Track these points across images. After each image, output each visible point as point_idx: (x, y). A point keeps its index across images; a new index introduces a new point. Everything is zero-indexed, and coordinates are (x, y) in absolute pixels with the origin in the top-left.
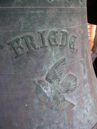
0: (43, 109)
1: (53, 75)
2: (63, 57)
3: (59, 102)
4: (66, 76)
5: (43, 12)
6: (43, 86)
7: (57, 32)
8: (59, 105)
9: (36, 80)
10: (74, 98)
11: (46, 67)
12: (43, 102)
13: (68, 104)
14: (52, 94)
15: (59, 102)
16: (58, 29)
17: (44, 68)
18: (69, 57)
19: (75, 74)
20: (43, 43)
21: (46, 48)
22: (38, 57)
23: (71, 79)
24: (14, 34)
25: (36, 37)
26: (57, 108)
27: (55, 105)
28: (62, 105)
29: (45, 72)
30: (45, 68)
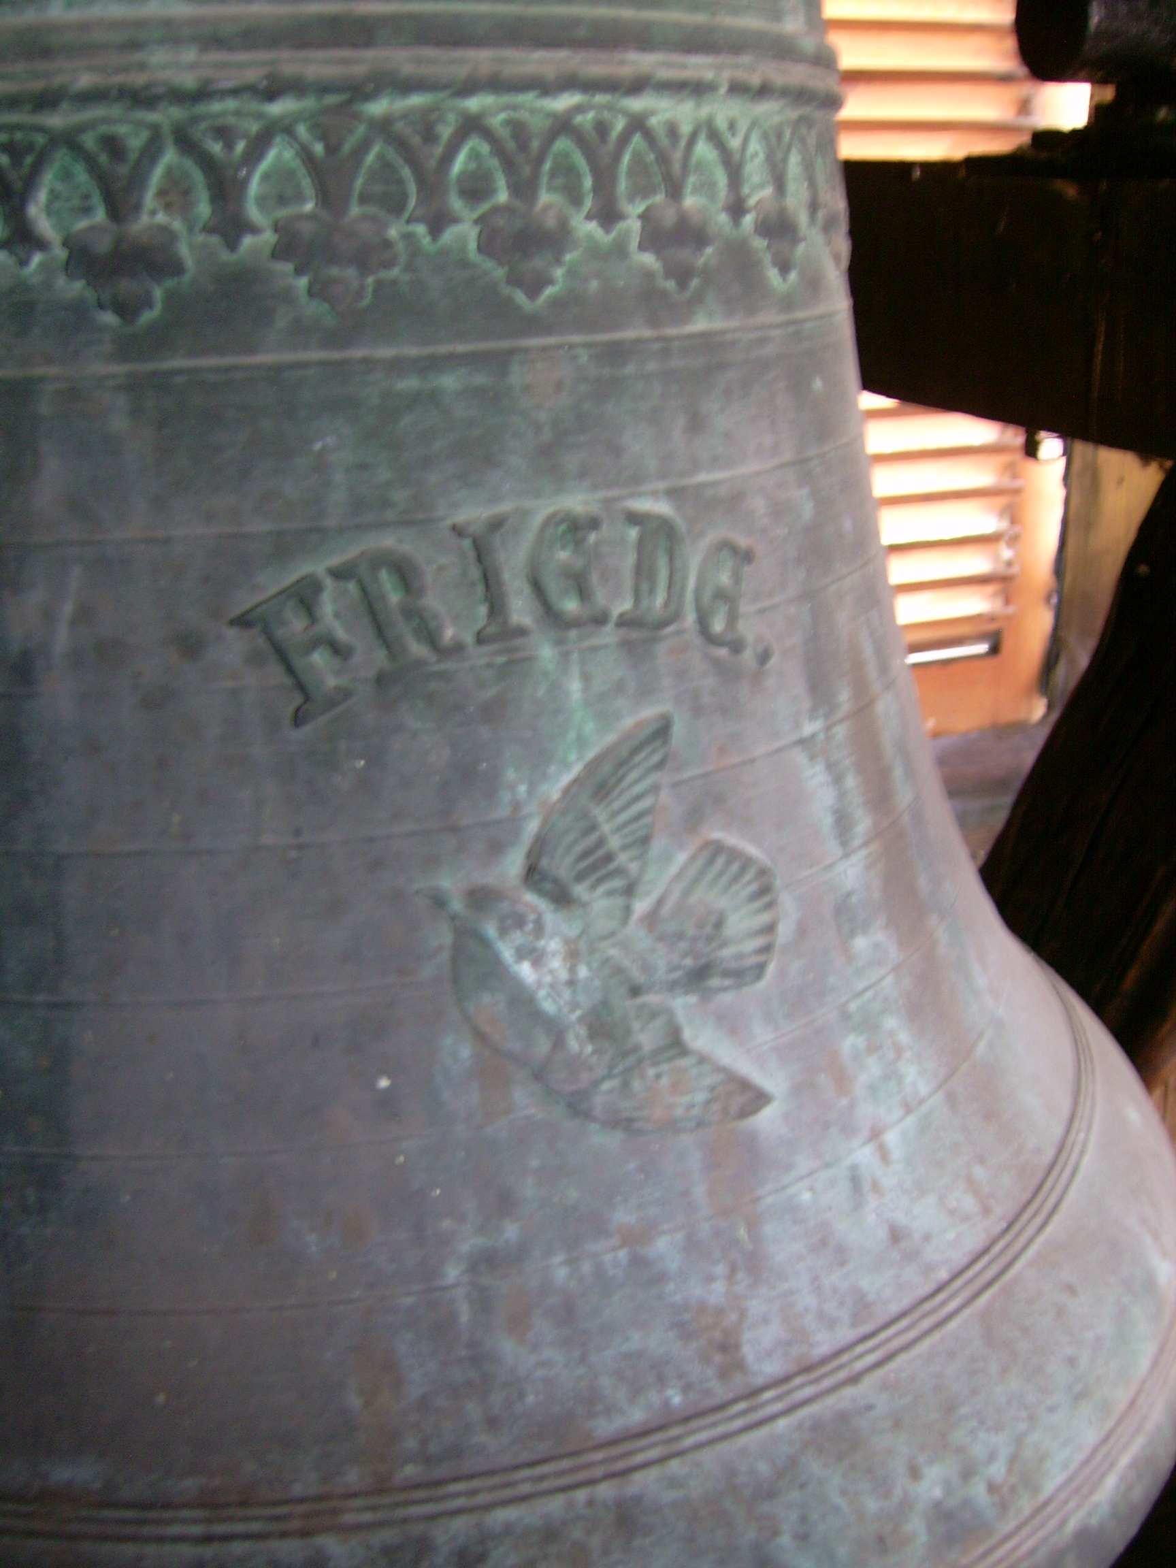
1: (579, 848)
2: (649, 712)
3: (640, 1061)
4: (681, 858)
10: (763, 1035)
14: (581, 998)
17: (506, 797)
18: (697, 711)
21: (518, 642)
23: (724, 880)
28: (665, 1081)
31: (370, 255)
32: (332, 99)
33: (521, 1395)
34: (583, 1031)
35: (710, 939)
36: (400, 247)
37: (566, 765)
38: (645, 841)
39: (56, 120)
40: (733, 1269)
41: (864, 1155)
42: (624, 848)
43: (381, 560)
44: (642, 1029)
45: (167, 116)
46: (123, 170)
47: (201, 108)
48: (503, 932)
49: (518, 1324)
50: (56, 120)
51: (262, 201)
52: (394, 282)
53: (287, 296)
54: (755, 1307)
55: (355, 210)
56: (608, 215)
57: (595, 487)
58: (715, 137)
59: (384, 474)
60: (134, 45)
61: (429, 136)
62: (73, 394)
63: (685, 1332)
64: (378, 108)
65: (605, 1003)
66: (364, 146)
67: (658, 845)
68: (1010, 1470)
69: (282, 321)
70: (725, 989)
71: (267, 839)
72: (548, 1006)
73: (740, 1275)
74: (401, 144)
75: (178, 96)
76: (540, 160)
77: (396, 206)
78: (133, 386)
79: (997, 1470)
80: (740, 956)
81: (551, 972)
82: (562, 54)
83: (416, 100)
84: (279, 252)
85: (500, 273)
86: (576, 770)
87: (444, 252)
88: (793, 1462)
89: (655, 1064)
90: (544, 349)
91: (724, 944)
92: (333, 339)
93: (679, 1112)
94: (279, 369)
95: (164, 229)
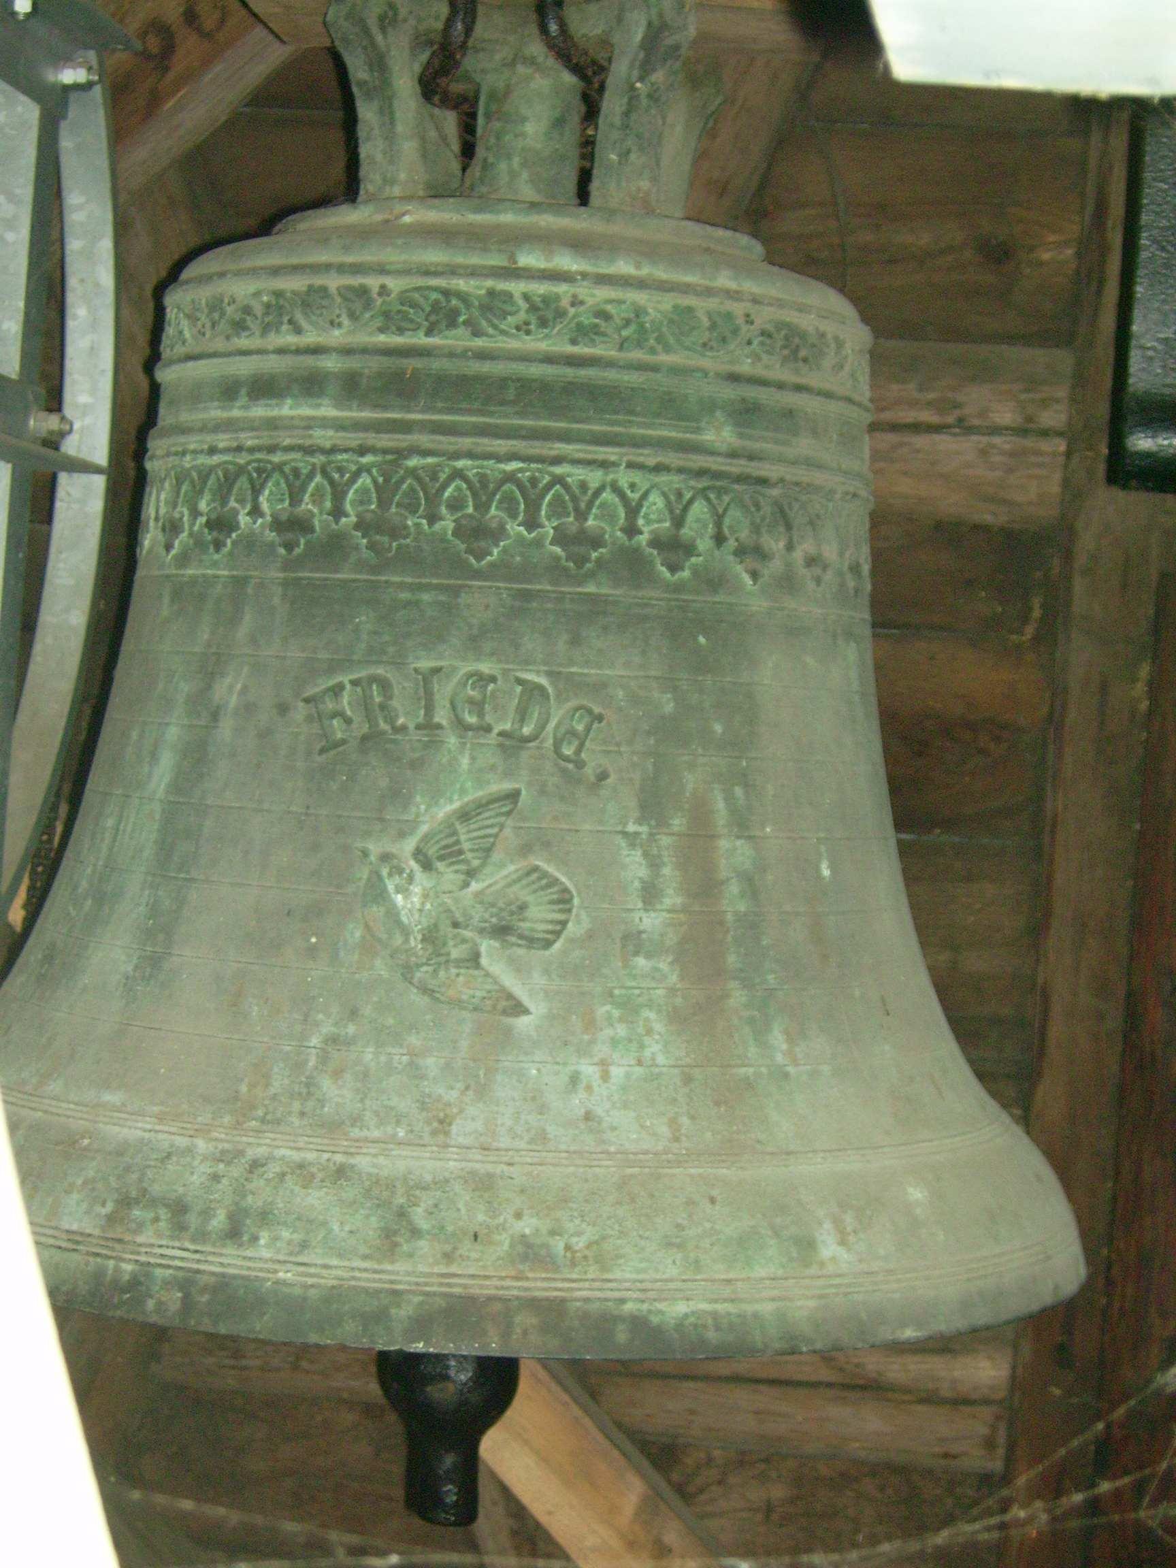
0: (371, 968)
1: (443, 843)
2: (507, 786)
3: (447, 961)
4: (512, 868)
5: (442, 598)
6: (390, 875)
7: (493, 679)
8: (442, 974)
9: (375, 848)
10: (539, 979)
11: (423, 807)
12: (380, 941)
13: (488, 987)
14: (423, 920)
15: (447, 961)
16: (504, 670)
17: (414, 809)
18: (543, 792)
19: (570, 879)
20: (429, 708)
21: (437, 732)
22: (399, 759)
23: (535, 886)
24: (333, 667)
25: (406, 685)
26: (434, 982)
27: (424, 968)
28: (461, 978)
29: (415, 824)
30: (418, 807)
31: (396, 532)
32: (389, 457)
33: (323, 1107)
34: (419, 937)
35: (512, 913)
36: (412, 530)
37: (451, 801)
38: (488, 851)
39: (277, 458)
40: (467, 1088)
41: (589, 1070)
42: (472, 850)
43: (373, 679)
44: (455, 946)
45: (319, 459)
46: (298, 483)
47: (332, 458)
48: (390, 875)
49: (337, 1074)
50: (277, 458)
51: (353, 503)
52: (407, 546)
53: (357, 548)
54: (471, 1111)
55: (393, 510)
56: (532, 523)
57: (500, 661)
58: (616, 489)
59: (386, 638)
60: (309, 428)
61: (434, 478)
62: (261, 585)
63: (423, 1107)
64: (413, 462)
65: (436, 925)
66: (402, 481)
67: (496, 856)
68: (588, 1247)
69: (353, 558)
70: (519, 946)
71: (294, 808)
72: (405, 919)
73: (470, 1093)
74: (419, 479)
75: (323, 451)
76: (494, 494)
77: (413, 509)
78: (285, 584)
79: (579, 1243)
80: (533, 930)
81: (412, 903)
82: (514, 442)
83: (430, 460)
84: (357, 526)
85: (463, 547)
86: (456, 805)
87: (433, 534)
88: (447, 1181)
89: (458, 967)
90: (480, 587)
91: (523, 920)
92: (375, 570)
93: (464, 997)
94: (345, 581)
95: (310, 511)
